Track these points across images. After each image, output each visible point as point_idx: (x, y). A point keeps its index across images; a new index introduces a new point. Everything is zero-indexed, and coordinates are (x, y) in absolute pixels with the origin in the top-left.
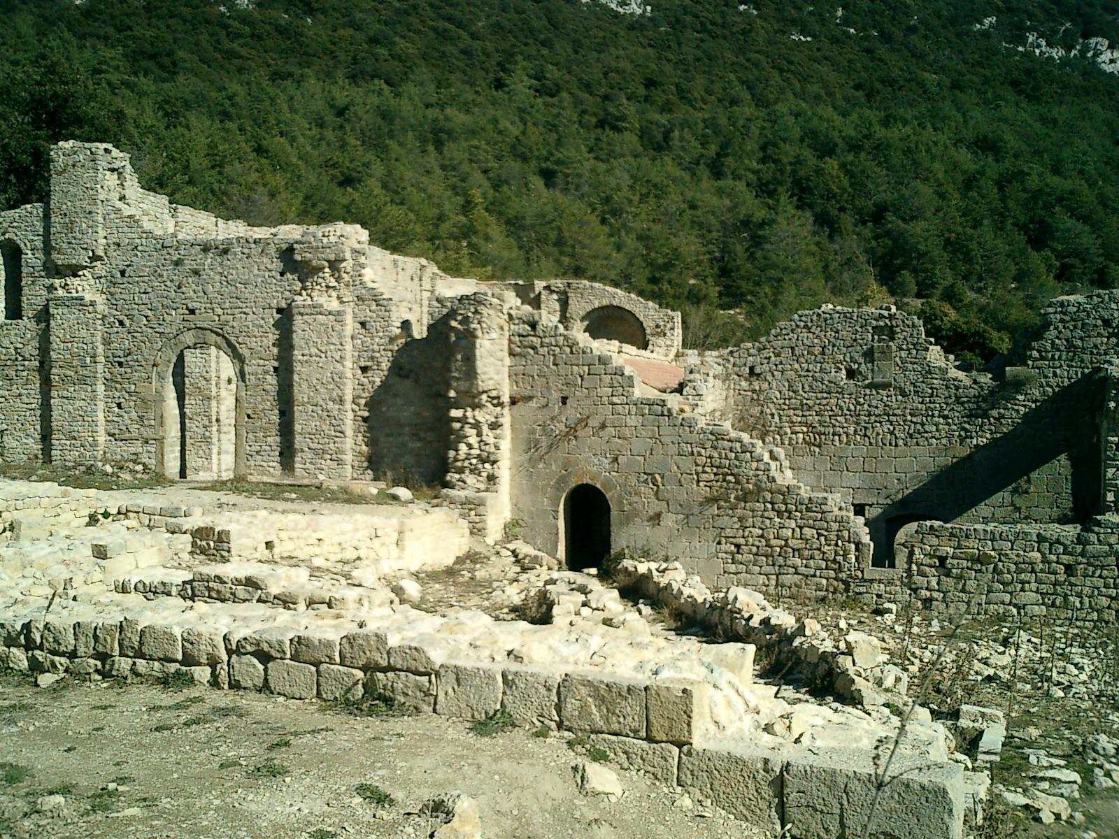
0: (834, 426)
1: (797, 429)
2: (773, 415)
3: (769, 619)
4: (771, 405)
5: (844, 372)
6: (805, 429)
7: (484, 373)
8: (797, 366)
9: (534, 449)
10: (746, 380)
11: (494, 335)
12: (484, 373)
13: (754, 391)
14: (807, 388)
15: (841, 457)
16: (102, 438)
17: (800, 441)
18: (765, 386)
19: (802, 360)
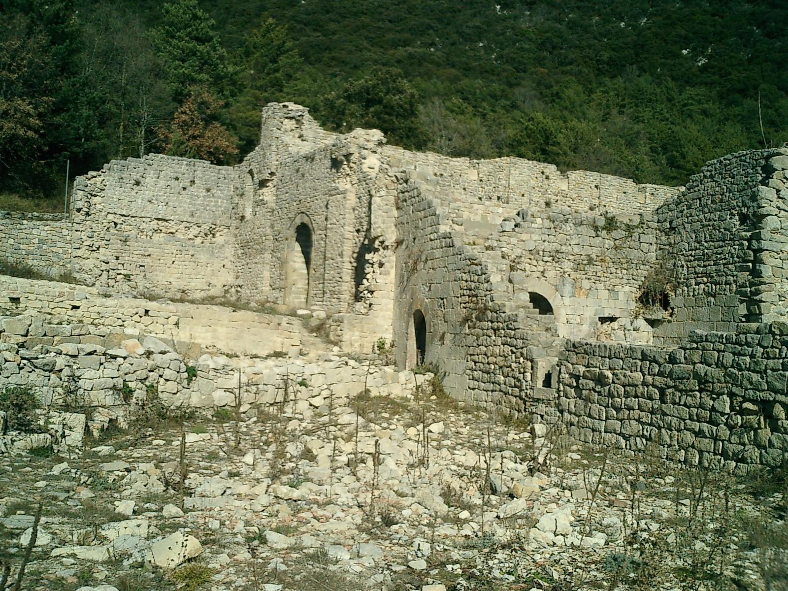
0: (727, 275)
1: (699, 280)
2: (682, 266)
3: (367, 391)
4: (682, 258)
5: (737, 217)
6: (705, 279)
7: (375, 223)
8: (702, 216)
9: (404, 282)
10: (666, 234)
11: (383, 193)
12: (375, 223)
13: (670, 244)
14: (708, 239)
15: (729, 307)
16: (267, 288)
17: (701, 291)
18: (678, 239)
19: (706, 210)
